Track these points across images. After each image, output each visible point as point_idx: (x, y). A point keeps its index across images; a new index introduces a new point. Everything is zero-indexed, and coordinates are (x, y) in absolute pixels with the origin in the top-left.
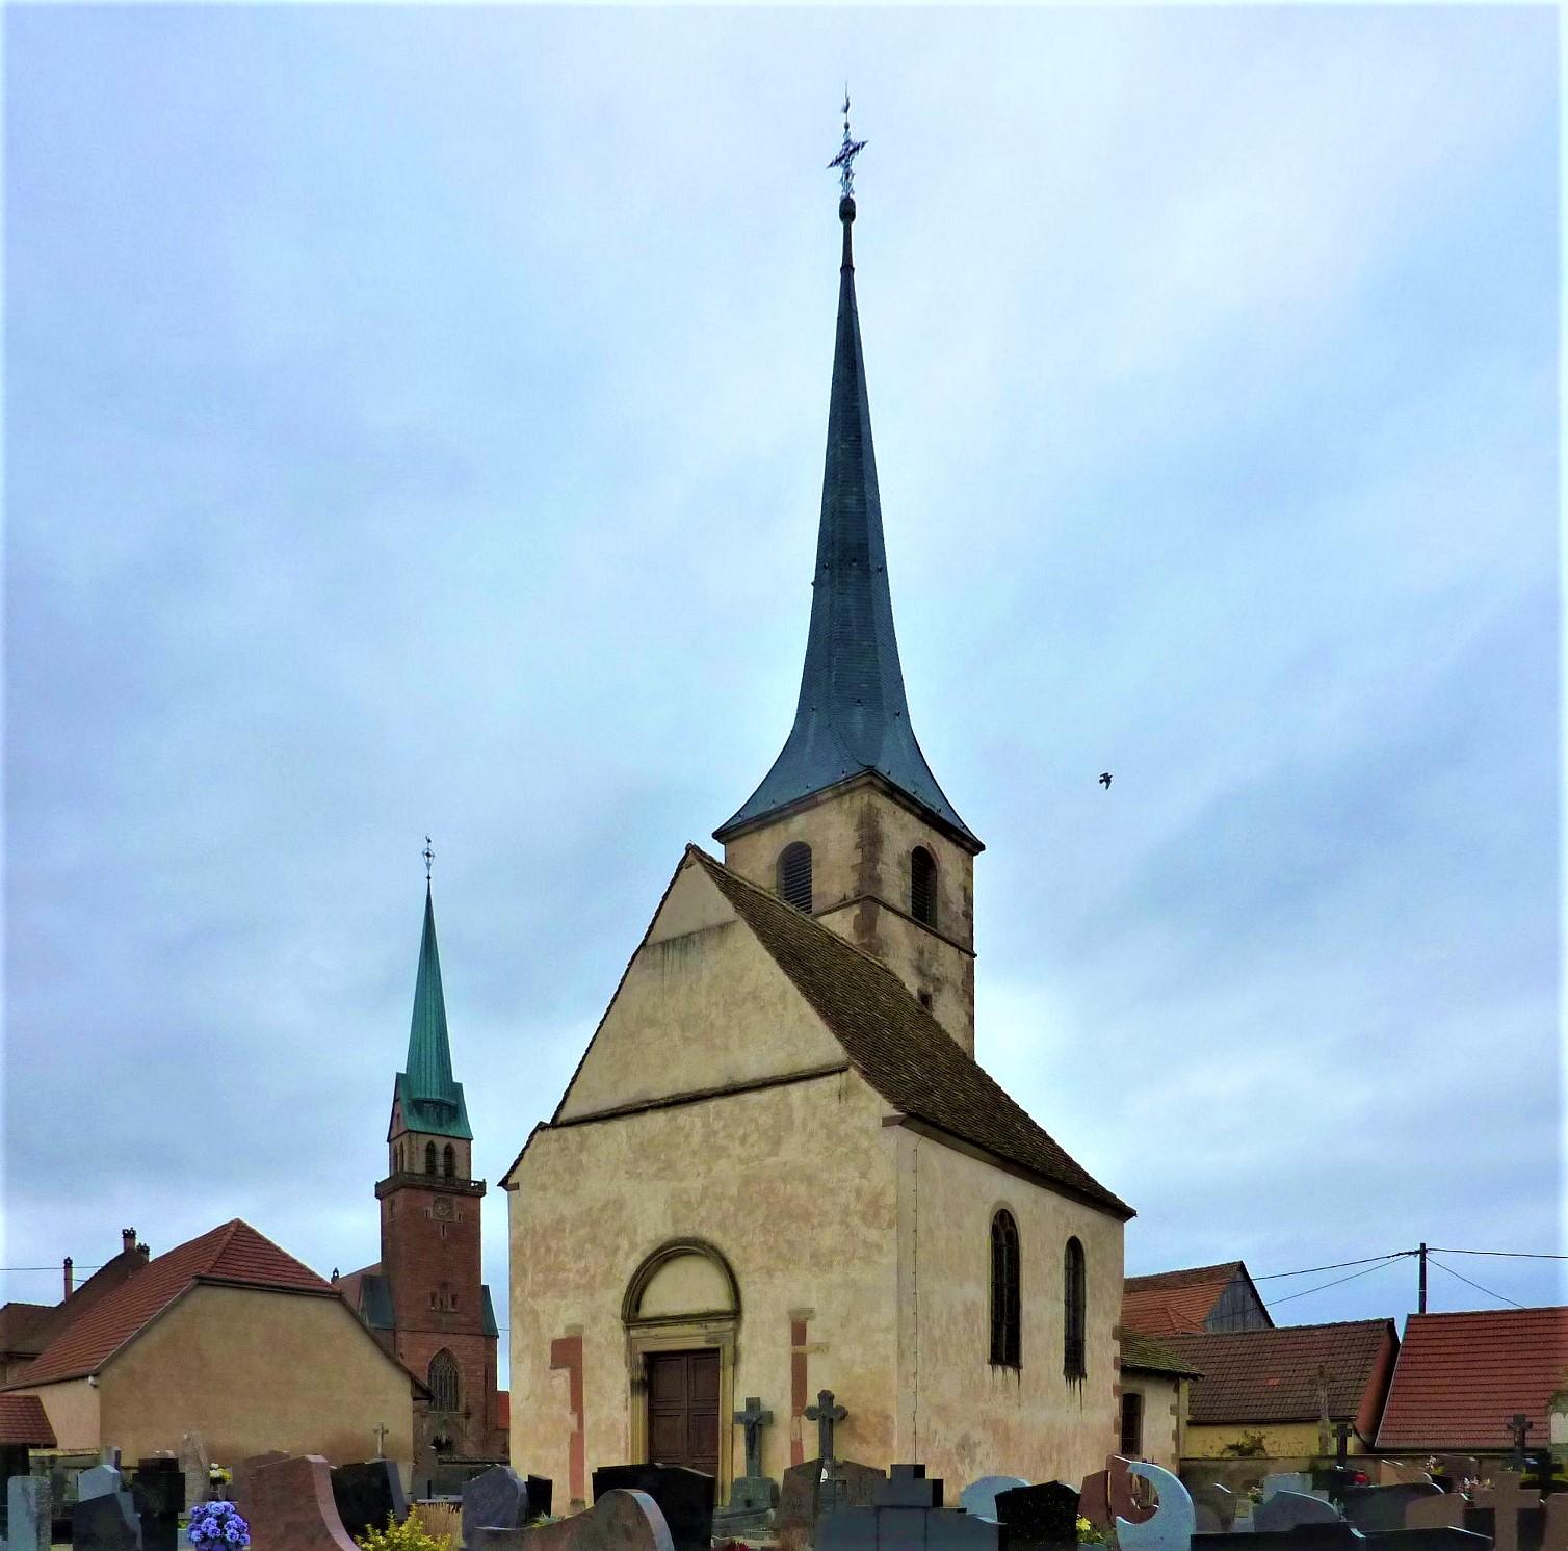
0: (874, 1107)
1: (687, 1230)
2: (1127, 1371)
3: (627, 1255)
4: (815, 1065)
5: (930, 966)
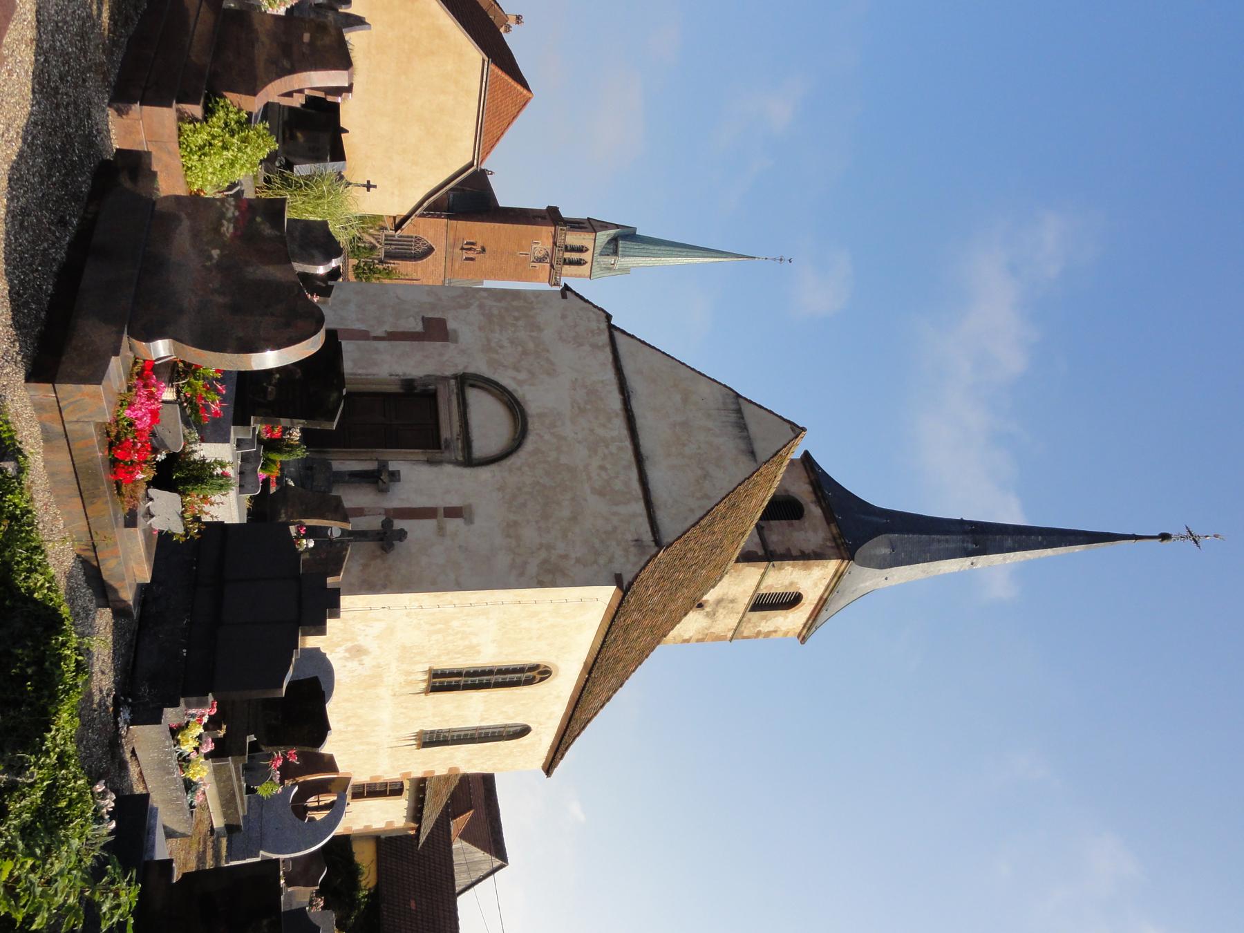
0: (629, 567)
1: (533, 425)
2: (420, 786)
3: (514, 379)
4: (658, 522)
5: (724, 608)
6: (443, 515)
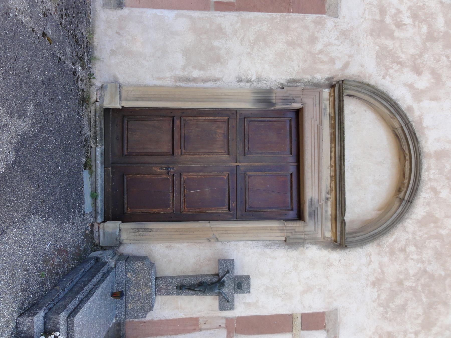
3: (411, 87)
6: (299, 327)
